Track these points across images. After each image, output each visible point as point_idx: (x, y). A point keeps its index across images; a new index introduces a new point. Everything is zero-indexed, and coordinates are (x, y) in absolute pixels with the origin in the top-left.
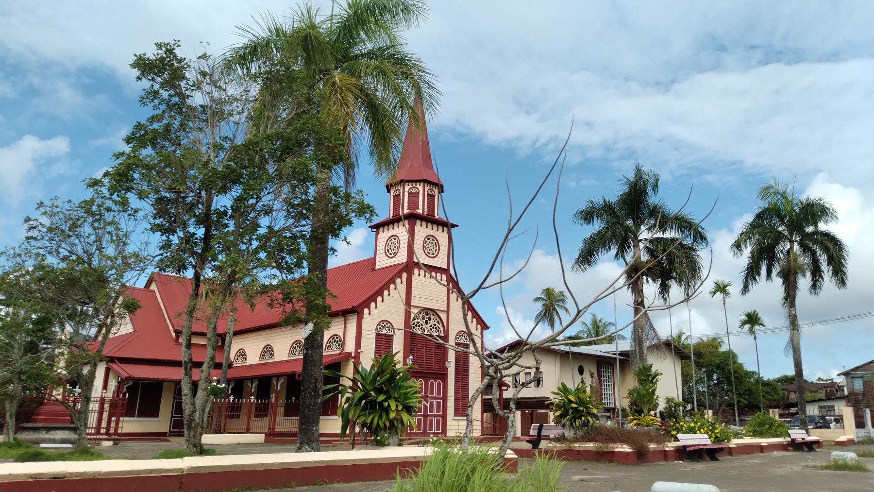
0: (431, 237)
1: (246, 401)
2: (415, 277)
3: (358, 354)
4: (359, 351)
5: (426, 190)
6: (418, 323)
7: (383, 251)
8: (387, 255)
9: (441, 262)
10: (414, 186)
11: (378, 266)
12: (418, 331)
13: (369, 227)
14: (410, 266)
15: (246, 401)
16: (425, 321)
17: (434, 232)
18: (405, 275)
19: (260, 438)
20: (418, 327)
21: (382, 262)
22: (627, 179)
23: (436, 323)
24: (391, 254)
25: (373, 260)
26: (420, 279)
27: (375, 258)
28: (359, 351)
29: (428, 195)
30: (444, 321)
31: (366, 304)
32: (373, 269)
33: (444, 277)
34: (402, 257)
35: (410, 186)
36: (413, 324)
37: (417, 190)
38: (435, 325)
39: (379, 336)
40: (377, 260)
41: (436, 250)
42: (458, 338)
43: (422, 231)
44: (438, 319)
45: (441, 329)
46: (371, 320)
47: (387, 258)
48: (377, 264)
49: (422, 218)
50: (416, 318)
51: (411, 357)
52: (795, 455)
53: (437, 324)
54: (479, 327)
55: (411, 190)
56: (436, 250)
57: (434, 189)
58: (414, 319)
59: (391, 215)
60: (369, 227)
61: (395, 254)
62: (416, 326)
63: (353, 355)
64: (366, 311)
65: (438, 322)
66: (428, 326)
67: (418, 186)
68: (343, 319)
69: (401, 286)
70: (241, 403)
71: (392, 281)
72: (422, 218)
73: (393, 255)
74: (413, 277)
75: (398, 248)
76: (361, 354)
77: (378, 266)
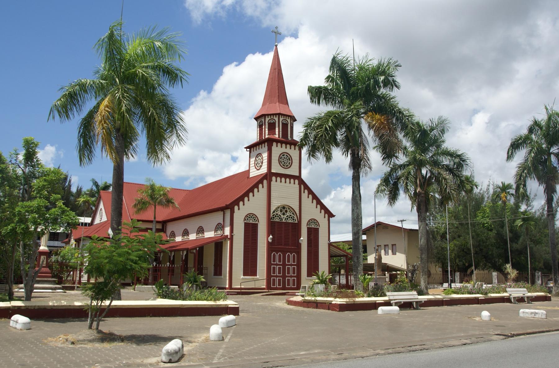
0: (285, 154)
1: (164, 265)
2: (273, 183)
3: (232, 236)
4: (232, 234)
5: (281, 121)
6: (277, 214)
7: (254, 165)
8: (256, 168)
9: (293, 171)
10: (272, 118)
11: (252, 175)
12: (277, 220)
13: (245, 148)
14: (269, 176)
15: (164, 265)
16: (282, 213)
17: (288, 150)
18: (265, 182)
19: (512, 295)
20: (277, 217)
21: (254, 173)
22: (102, 151)
23: (291, 214)
24: (258, 167)
25: (248, 172)
26: (276, 184)
27: (249, 170)
28: (232, 234)
29: (283, 124)
30: (296, 212)
31: (236, 202)
32: (248, 177)
33: (297, 181)
34: (264, 170)
35: (269, 118)
36: (273, 215)
37: (274, 120)
38: (291, 215)
39: (247, 225)
40: (251, 171)
41: (289, 163)
42: (310, 224)
43: (277, 150)
44: (293, 211)
45: (296, 218)
46: (240, 214)
47: (256, 170)
48: (251, 174)
49: (277, 141)
50: (275, 211)
51: (271, 237)
52: (297, 311)
53: (292, 215)
54: (327, 215)
55: (270, 121)
56: (289, 163)
57: (287, 119)
58: (274, 212)
59: (258, 139)
60: (245, 148)
61: (261, 166)
62: (276, 216)
63: (229, 237)
64: (236, 207)
65: (293, 214)
66: (285, 216)
67: (275, 118)
68: (222, 213)
69: (262, 191)
70: (161, 267)
71: (256, 186)
72: (277, 141)
73: (259, 168)
74: (272, 183)
75: (262, 163)
76: (234, 236)
77: (252, 175)
